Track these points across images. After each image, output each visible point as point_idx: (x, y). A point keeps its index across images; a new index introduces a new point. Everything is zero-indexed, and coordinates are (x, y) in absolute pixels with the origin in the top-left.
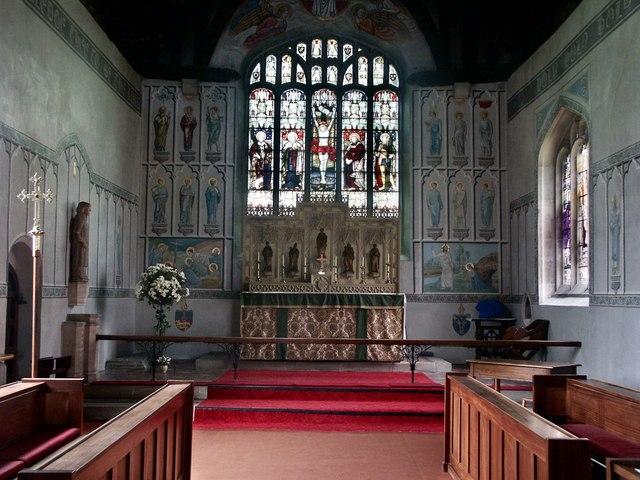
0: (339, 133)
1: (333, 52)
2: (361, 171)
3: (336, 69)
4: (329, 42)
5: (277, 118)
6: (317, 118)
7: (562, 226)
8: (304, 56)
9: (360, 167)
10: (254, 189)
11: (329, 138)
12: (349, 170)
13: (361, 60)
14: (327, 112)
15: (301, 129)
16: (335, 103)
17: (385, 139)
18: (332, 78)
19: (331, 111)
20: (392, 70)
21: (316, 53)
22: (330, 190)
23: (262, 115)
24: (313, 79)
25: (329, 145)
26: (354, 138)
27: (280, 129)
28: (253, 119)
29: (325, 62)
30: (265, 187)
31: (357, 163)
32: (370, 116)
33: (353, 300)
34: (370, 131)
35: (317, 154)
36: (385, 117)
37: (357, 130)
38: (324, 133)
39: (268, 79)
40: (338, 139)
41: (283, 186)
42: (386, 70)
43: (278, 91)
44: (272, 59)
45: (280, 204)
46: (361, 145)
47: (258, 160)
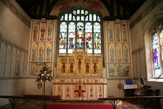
3: (83, 17)
8: (75, 14)
10: (61, 49)
11: (82, 35)
12: (87, 43)
13: (90, 15)
14: (81, 28)
16: (83, 25)
17: (97, 35)
19: (82, 28)
20: (98, 17)
22: (82, 49)
25: (82, 37)
26: (89, 35)
35: (78, 39)
38: (80, 33)
40: (84, 35)
42: (97, 17)
43: (68, 22)
47: (62, 41)
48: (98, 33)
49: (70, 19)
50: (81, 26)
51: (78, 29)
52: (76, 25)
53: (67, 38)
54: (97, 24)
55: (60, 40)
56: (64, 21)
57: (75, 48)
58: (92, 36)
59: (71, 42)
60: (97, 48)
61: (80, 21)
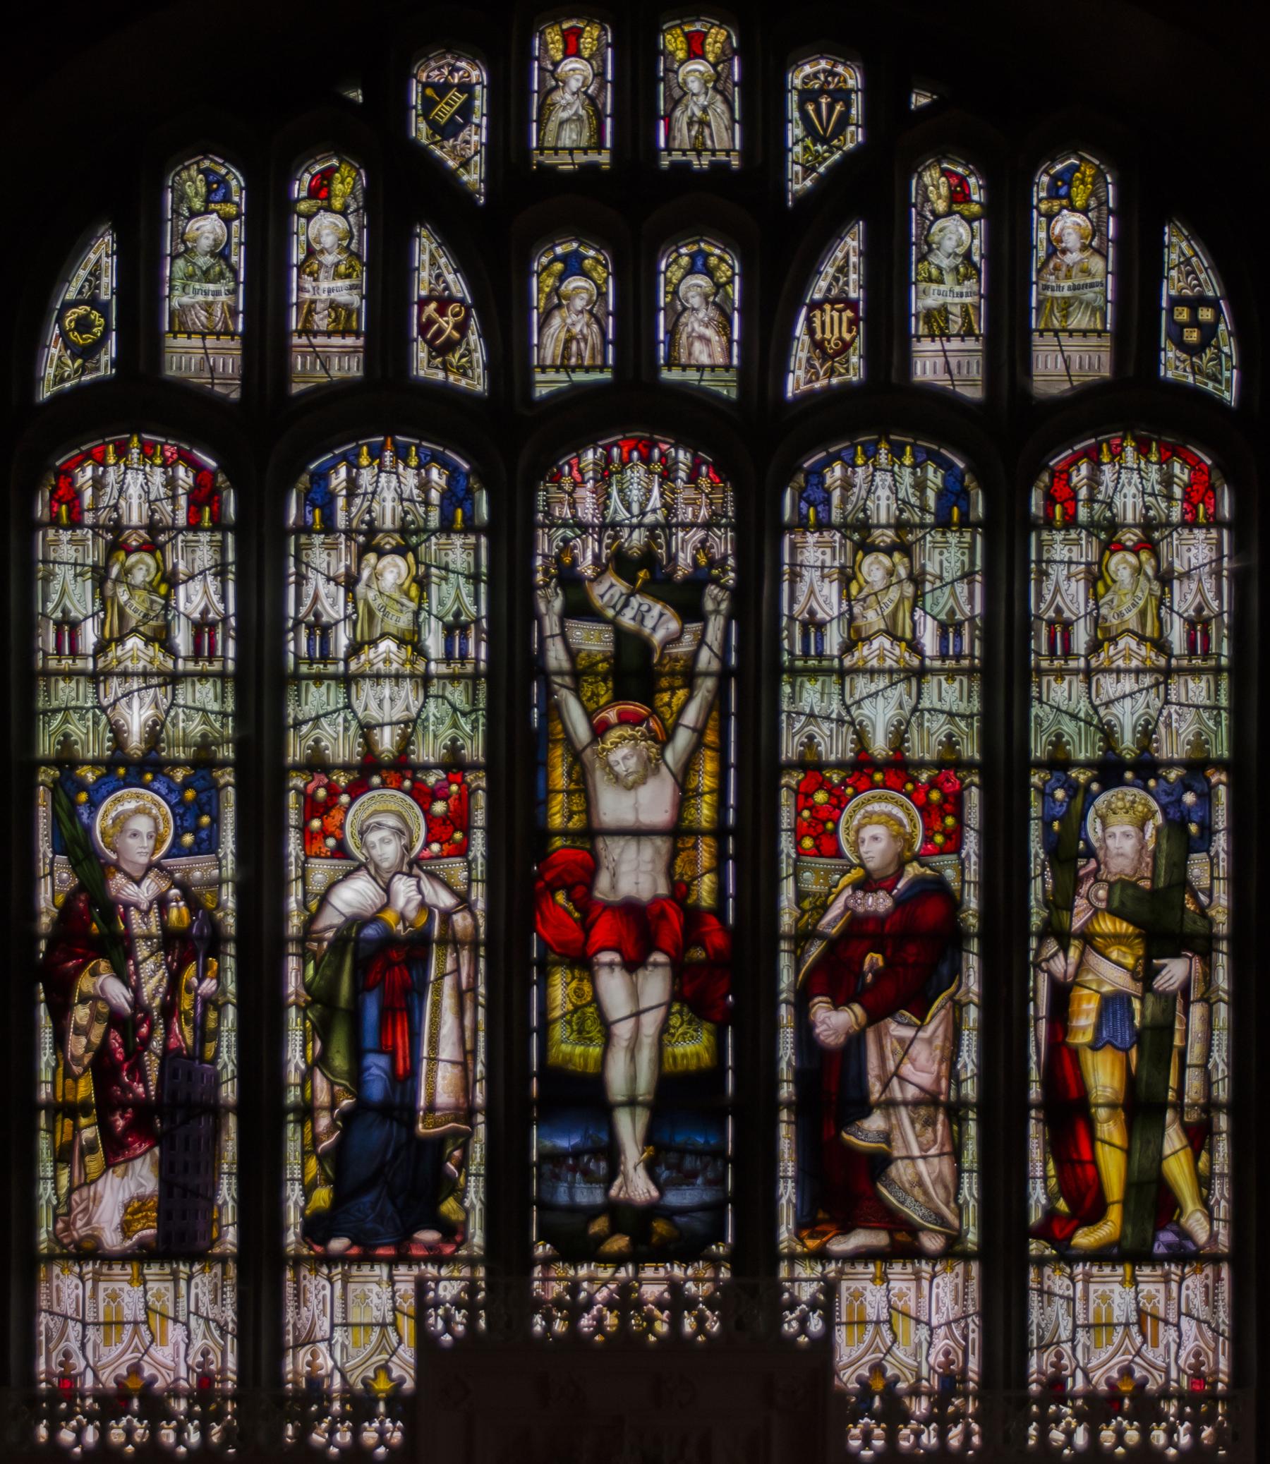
0: (757, 794)
1: (701, 110)
2: (929, 1100)
3: (728, 266)
4: (673, 42)
5: (261, 685)
6: (578, 674)
8: (467, 157)
9: (922, 1070)
10: (88, 1252)
11: (678, 833)
12: (836, 1086)
13: (933, 183)
14: (658, 622)
15: (454, 764)
16: (722, 543)
17: (1122, 834)
18: (702, 345)
19: (691, 611)
20: (1185, 265)
21: (569, 129)
22: (687, 1249)
23: (878, 651)
24: (548, 343)
25: (680, 889)
26: (876, 829)
27: (281, 773)
28: (65, 691)
29: (636, 205)
30: (174, 1238)
31: (897, 1030)
32: (1006, 656)
34: (1005, 778)
35: (583, 964)
36: (878, 651)
37: (898, 769)
38: (635, 806)
39: (184, 357)
40: (748, 841)
41: (317, 1228)
42: (1138, 268)
43: (263, 452)
44: (216, 189)
45: (295, 1365)
46: (936, 892)
47: (115, 1019)
48: (1147, 767)
49: (1068, 358)
50: (645, 570)
51: (556, 656)
52: (989, 526)
53: (244, 937)
54: (1129, 483)
55: (60, 1014)
56: (142, 402)
57: (477, 1238)
58: (964, 871)
59: (377, 1065)
60: (1109, 1229)
61: (637, 402)
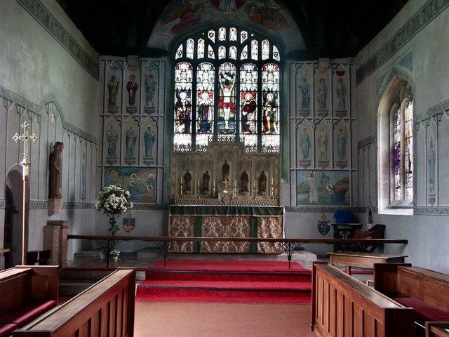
0: (238, 93)
1: (233, 37)
2: (253, 120)
3: (236, 48)
4: (231, 30)
5: (195, 83)
6: (223, 83)
7: (395, 159)
8: (213, 39)
9: (252, 117)
10: (178, 133)
11: (231, 97)
12: (245, 119)
13: (253, 42)
14: (229, 78)
15: (211, 90)
16: (235, 72)
17: (270, 97)
18: (233, 55)
19: (232, 78)
20: (275, 49)
21: (222, 37)
22: (231, 133)
23: (184, 81)
24: (220, 55)
25: (231, 102)
26: (248, 97)
27: (196, 91)
28: (177, 84)
29: (228, 44)
30: (186, 131)
31: (250, 114)
32: (260, 82)
33: (248, 211)
34: (260, 92)
35: (223, 108)
36: (270, 82)
37: (250, 91)
38: (227, 94)
39: (188, 56)
40: (237, 97)
41: (199, 131)
42: (271, 49)
43: (195, 64)
44: (191, 41)
45: (197, 143)
46: (253, 102)
47: (181, 112)
